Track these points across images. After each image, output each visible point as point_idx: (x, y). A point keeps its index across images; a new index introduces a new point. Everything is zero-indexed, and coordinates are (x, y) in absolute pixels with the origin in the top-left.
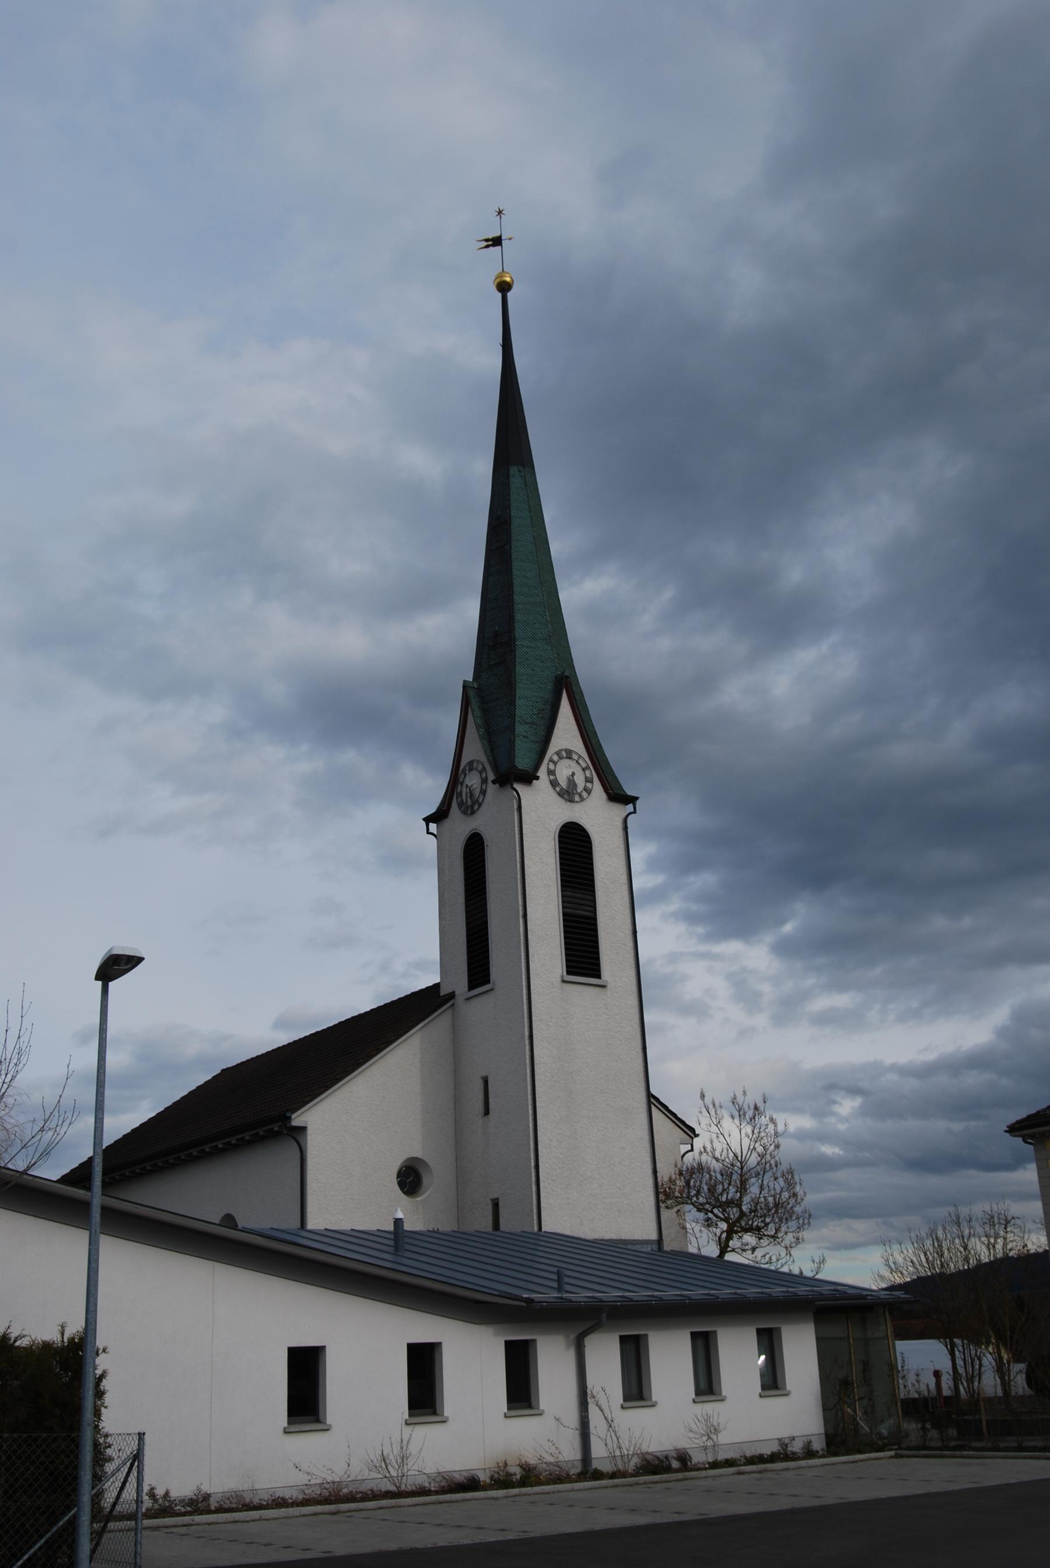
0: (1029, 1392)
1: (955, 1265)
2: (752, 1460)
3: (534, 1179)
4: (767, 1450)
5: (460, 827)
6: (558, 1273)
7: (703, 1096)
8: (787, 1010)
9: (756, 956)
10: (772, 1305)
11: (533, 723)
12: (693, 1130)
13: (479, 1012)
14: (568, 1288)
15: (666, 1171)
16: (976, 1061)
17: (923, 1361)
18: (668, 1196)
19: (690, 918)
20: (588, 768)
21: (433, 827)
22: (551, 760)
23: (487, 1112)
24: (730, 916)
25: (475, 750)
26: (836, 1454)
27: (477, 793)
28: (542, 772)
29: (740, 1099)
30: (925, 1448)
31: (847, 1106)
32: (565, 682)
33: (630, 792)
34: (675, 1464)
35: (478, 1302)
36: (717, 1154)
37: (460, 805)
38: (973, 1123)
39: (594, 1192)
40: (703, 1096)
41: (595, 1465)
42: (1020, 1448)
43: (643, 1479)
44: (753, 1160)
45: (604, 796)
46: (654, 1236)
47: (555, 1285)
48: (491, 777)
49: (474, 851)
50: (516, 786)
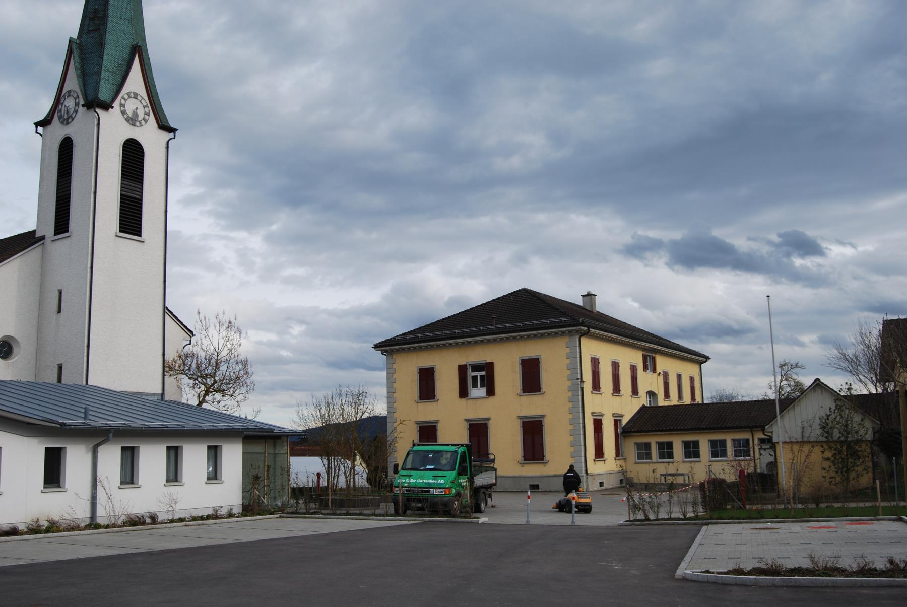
0: (367, 485)
1: (336, 419)
2: (194, 519)
3: (85, 353)
4: (205, 513)
5: (58, 132)
6: (85, 408)
7: (199, 313)
8: (269, 274)
9: (255, 241)
10: (217, 434)
11: (114, 72)
12: (192, 332)
13: (60, 250)
14: (90, 417)
15: (171, 355)
16: (370, 312)
17: (306, 469)
18: (171, 369)
19: (218, 215)
20: (147, 106)
21: (40, 129)
22: (123, 98)
23: (59, 311)
24: (241, 217)
25: (73, 83)
26: (246, 516)
27: (71, 111)
28: (116, 104)
29: (221, 317)
30: (297, 513)
31: (297, 330)
32: (138, 50)
33: (173, 125)
34: (148, 520)
35: (29, 423)
36: (204, 347)
37: (60, 118)
38: (364, 345)
39: (124, 363)
40: (199, 313)
41: (100, 521)
42: (347, 514)
43: (126, 529)
44: (224, 353)
45: (156, 125)
46: (160, 392)
47: (83, 415)
48: (82, 102)
49: (66, 148)
50: (97, 110)
